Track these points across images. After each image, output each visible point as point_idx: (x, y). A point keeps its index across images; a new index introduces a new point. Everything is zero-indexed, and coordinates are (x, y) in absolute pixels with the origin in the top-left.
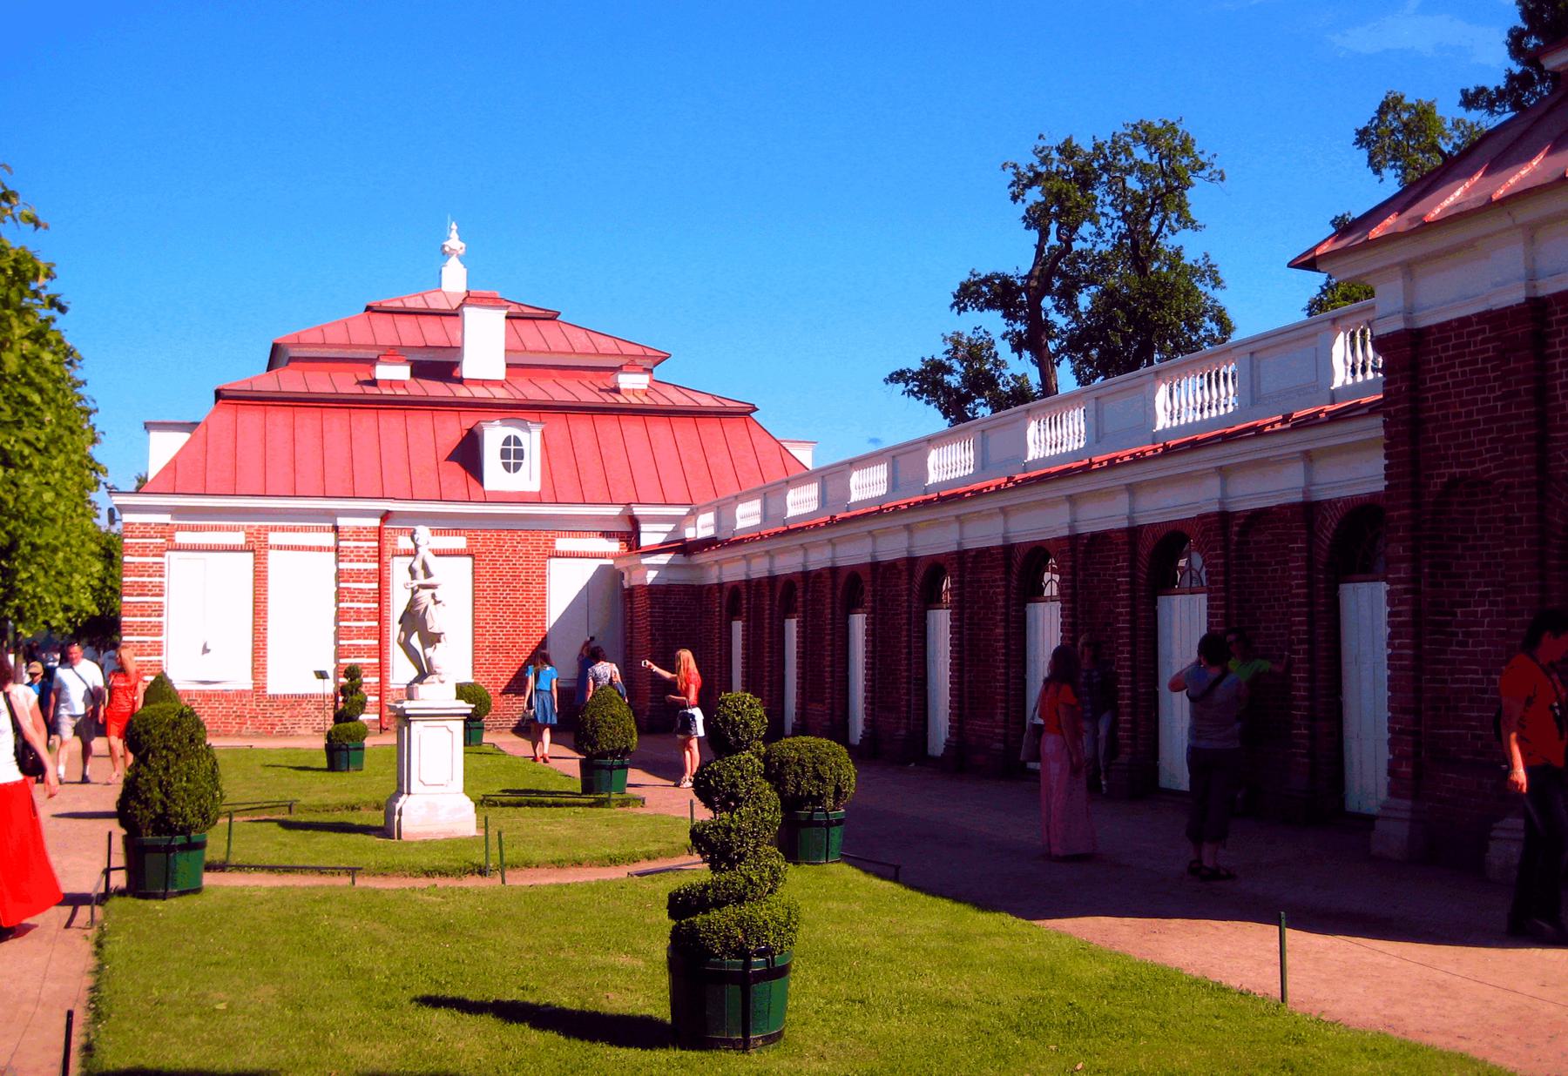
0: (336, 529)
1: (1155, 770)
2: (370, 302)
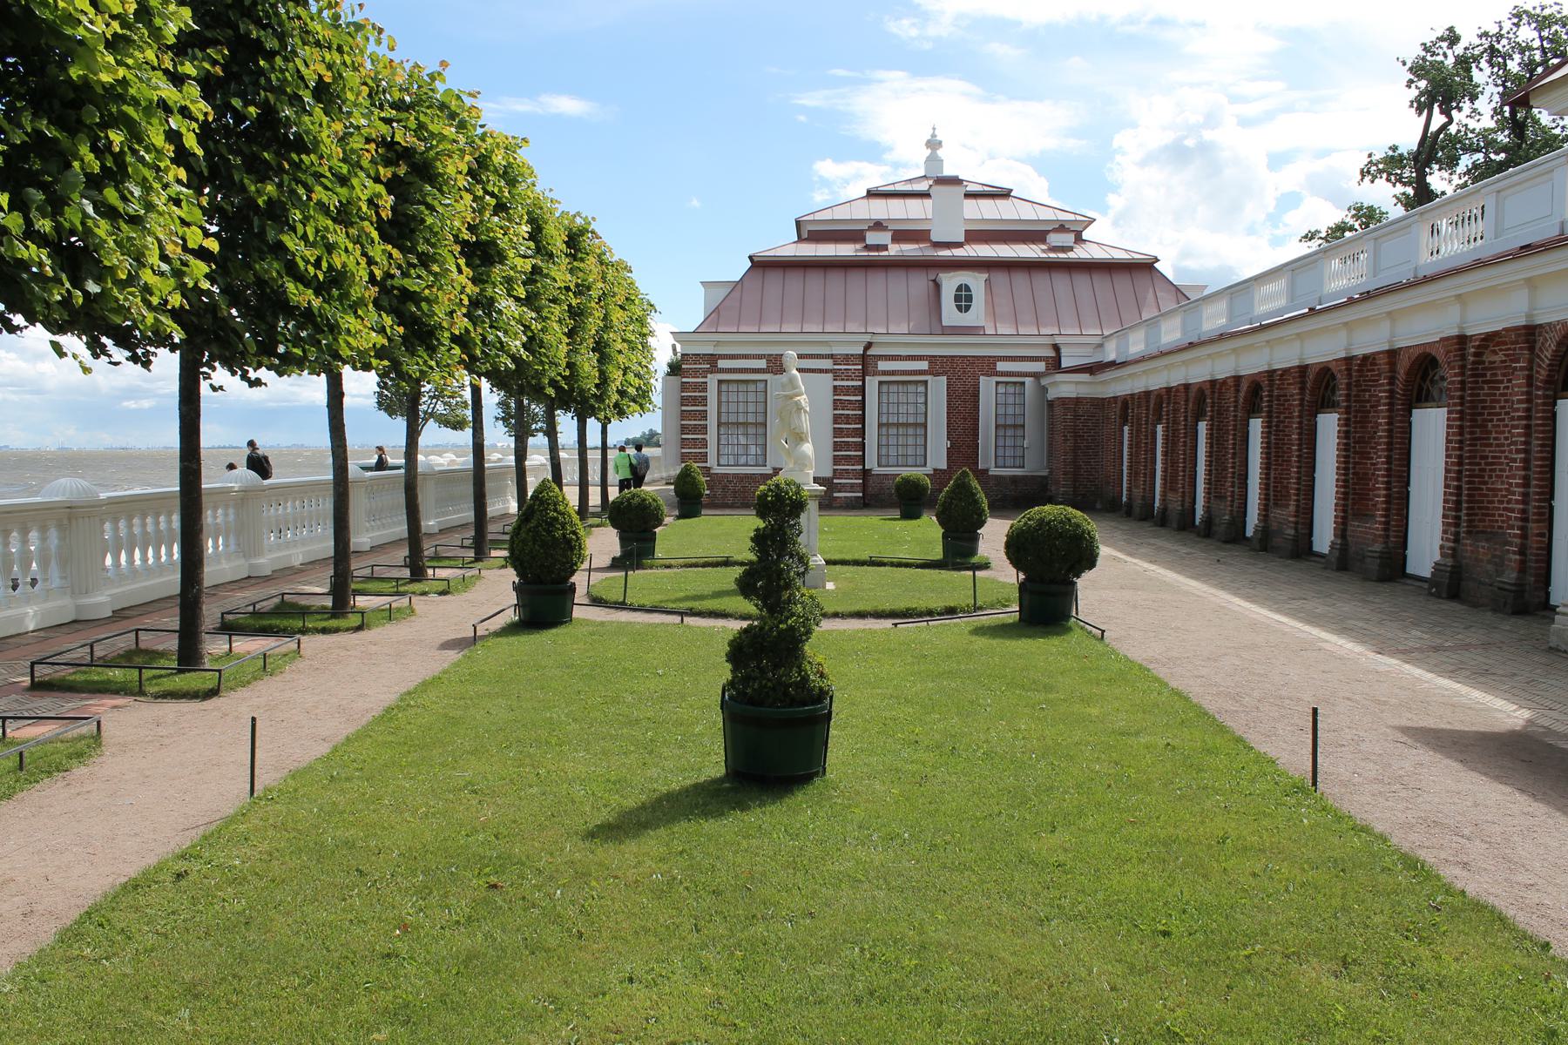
1: (1311, 543)
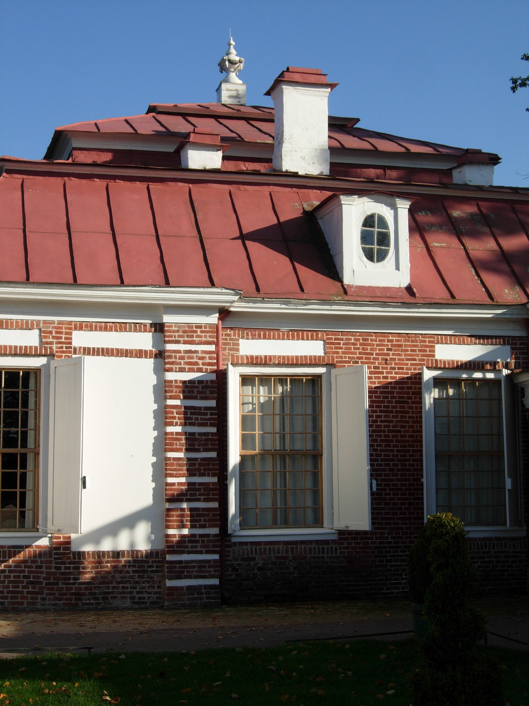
0: (159, 328)
2: (128, 118)
